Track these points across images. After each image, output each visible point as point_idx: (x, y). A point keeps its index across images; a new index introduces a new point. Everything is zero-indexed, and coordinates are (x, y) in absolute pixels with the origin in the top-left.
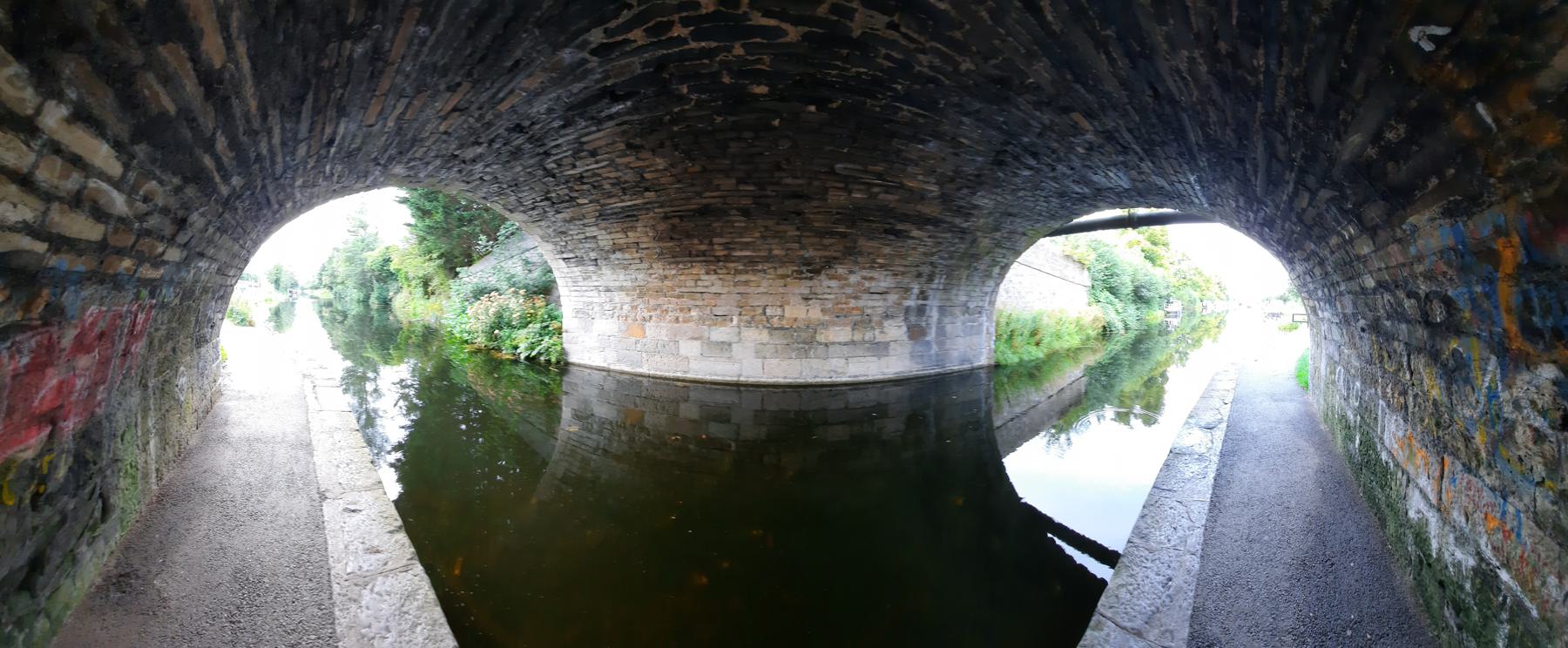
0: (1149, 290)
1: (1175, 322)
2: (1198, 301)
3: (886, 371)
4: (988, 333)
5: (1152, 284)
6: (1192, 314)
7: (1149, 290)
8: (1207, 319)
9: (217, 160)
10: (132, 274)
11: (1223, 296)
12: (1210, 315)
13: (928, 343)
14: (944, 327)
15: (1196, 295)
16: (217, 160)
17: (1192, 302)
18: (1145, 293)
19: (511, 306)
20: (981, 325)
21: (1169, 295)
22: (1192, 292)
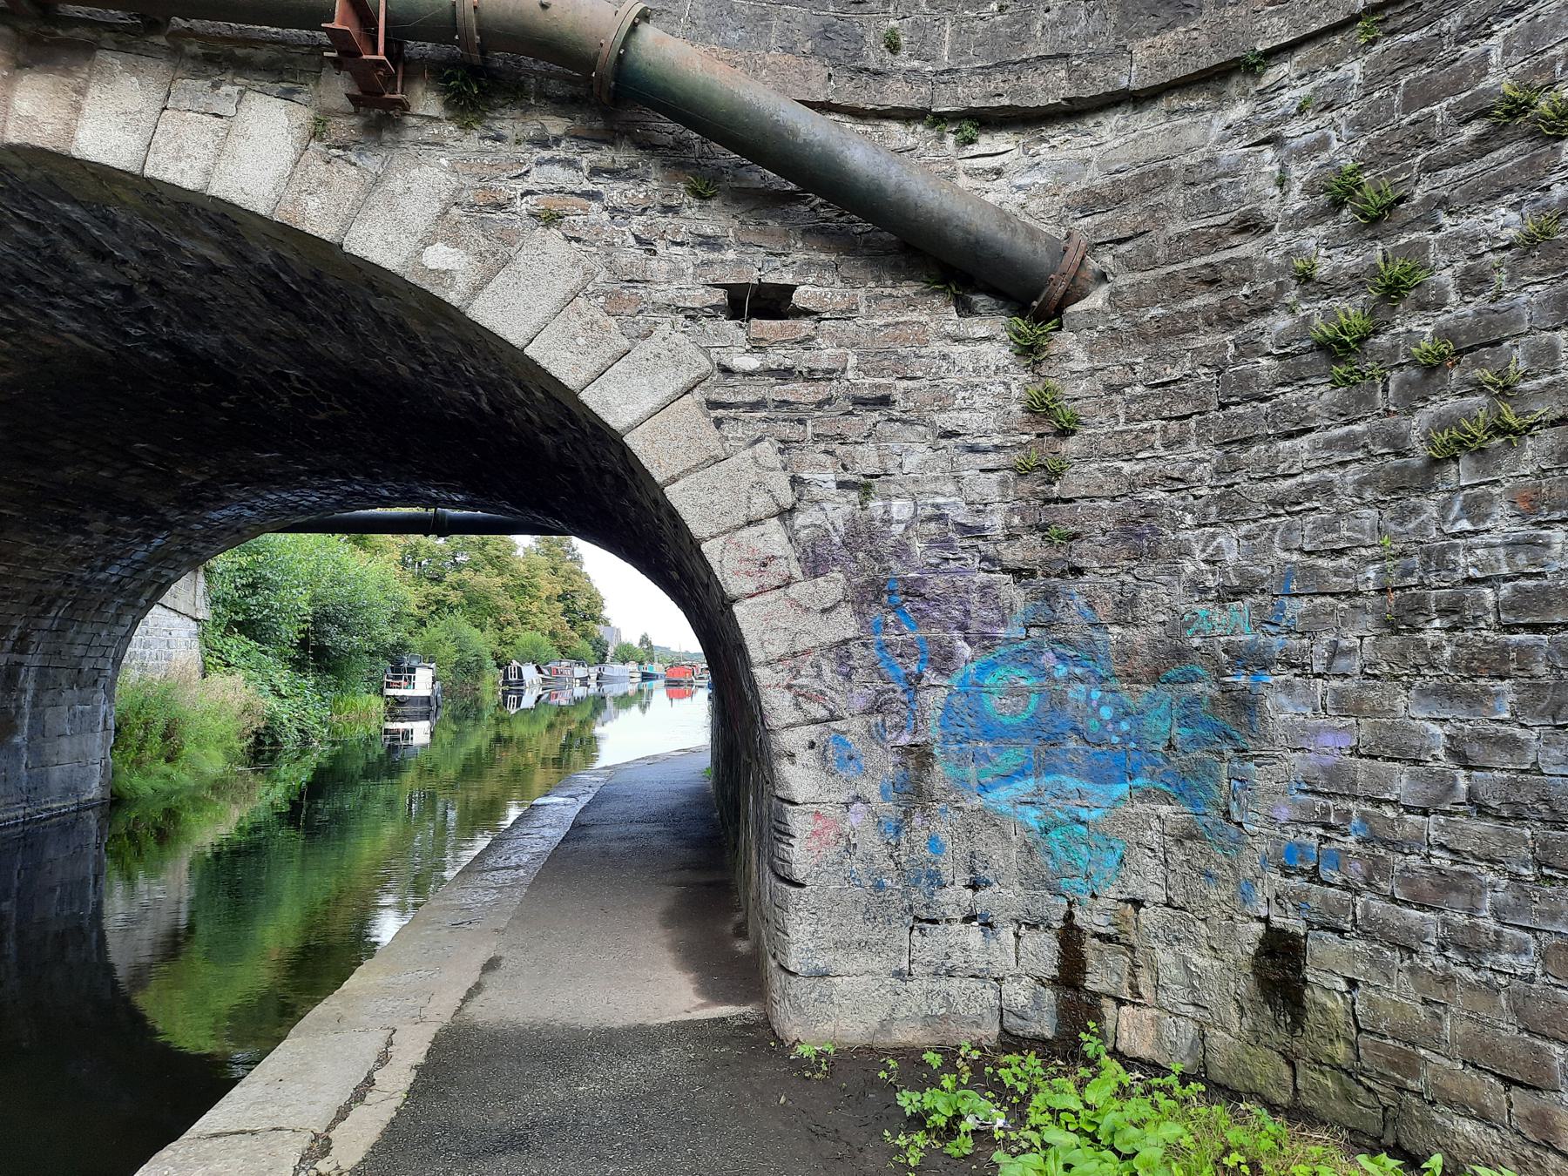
0: (345, 628)
1: (420, 732)
2: (490, 663)
3: (272, 1065)
4: (105, 729)
5: (355, 610)
6: (468, 711)
7: (345, 628)
8: (521, 729)
9: (253, 315)
10: (1032, 197)
11: (581, 645)
12: (531, 715)
13: (17, 749)
14: (42, 713)
15: (482, 641)
16: (253, 315)
17: (469, 669)
18: (334, 638)
19: (576, 694)
20: (95, 710)
21: (401, 647)
22: (467, 630)
